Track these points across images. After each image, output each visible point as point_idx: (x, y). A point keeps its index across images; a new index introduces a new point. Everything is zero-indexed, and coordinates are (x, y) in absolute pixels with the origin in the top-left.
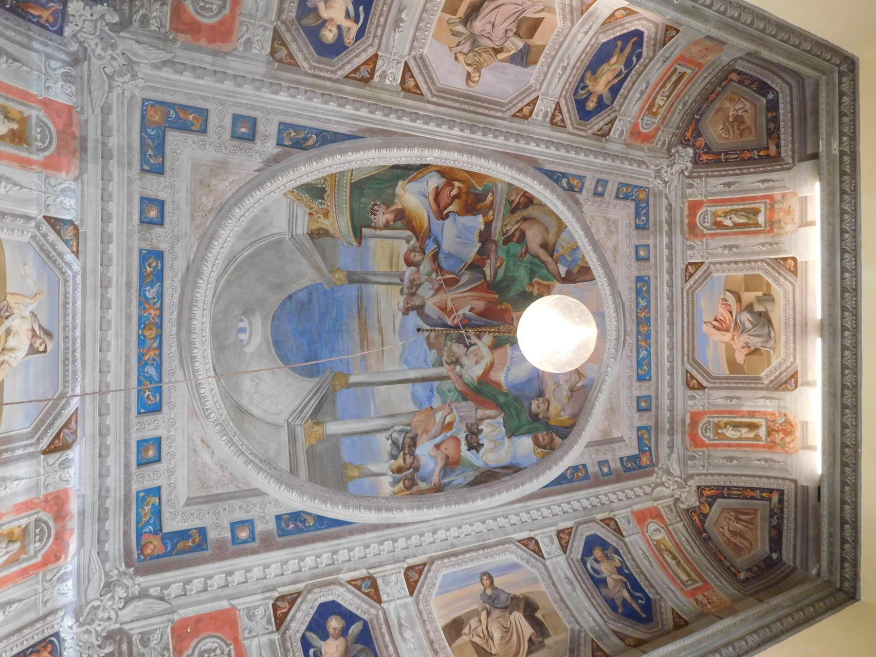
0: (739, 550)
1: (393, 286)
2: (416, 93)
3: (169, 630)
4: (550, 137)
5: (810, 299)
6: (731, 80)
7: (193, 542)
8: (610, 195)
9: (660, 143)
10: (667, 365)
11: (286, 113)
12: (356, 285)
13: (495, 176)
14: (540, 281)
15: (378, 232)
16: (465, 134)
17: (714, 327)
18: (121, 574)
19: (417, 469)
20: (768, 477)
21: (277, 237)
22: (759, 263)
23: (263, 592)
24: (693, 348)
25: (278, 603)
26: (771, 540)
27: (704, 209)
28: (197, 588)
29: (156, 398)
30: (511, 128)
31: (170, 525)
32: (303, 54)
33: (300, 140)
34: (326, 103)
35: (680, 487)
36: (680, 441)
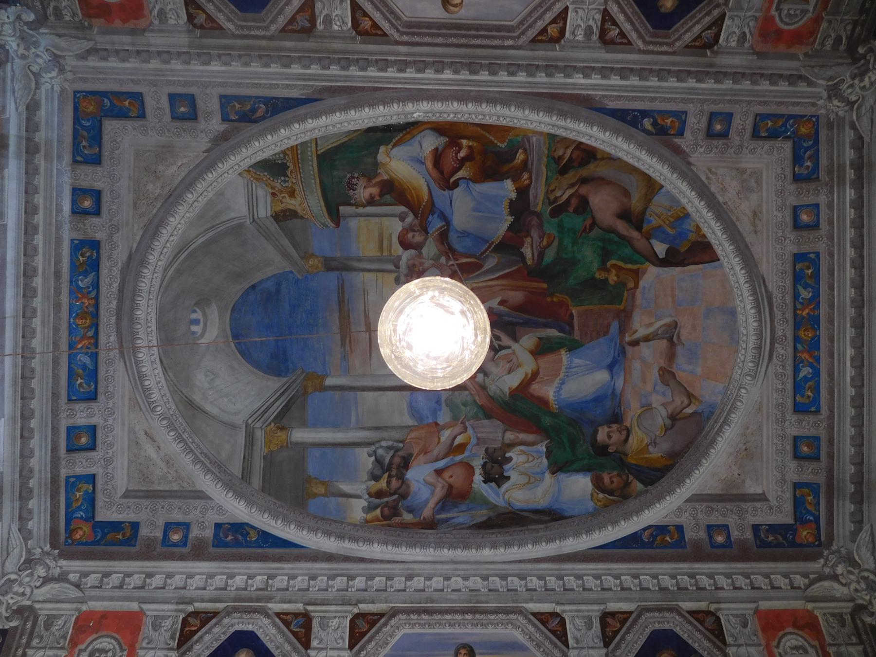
1: (385, 274)
2: (376, 35)
3: (73, 619)
4: (606, 61)
7: (123, 536)
9: (829, 43)
10: (851, 391)
12: (336, 273)
13: (525, 126)
14: (621, 264)
15: (361, 210)
19: (404, 496)
23: (177, 603)
25: (189, 619)
30: (534, 59)
31: (104, 514)
32: (225, 14)
33: (250, 113)
34: (267, 65)
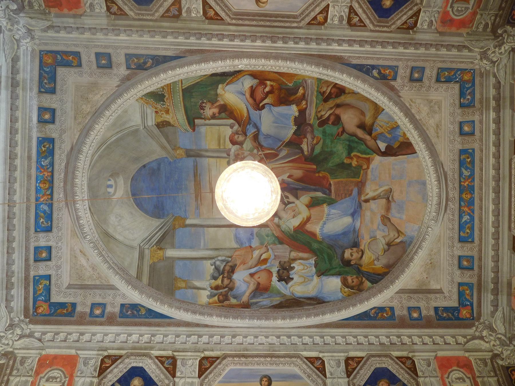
2: (217, 19)
3: (37, 359)
4: (351, 36)
7: (67, 310)
8: (430, 79)
9: (481, 27)
10: (492, 230)
11: (128, 48)
12: (193, 158)
13: (304, 74)
15: (207, 122)
16: (267, 45)
18: (20, 321)
19: (231, 289)
21: (134, 128)
28: (60, 338)
29: (48, 223)
31: (55, 298)
32: (128, 6)
33: (142, 64)
35: (503, 344)
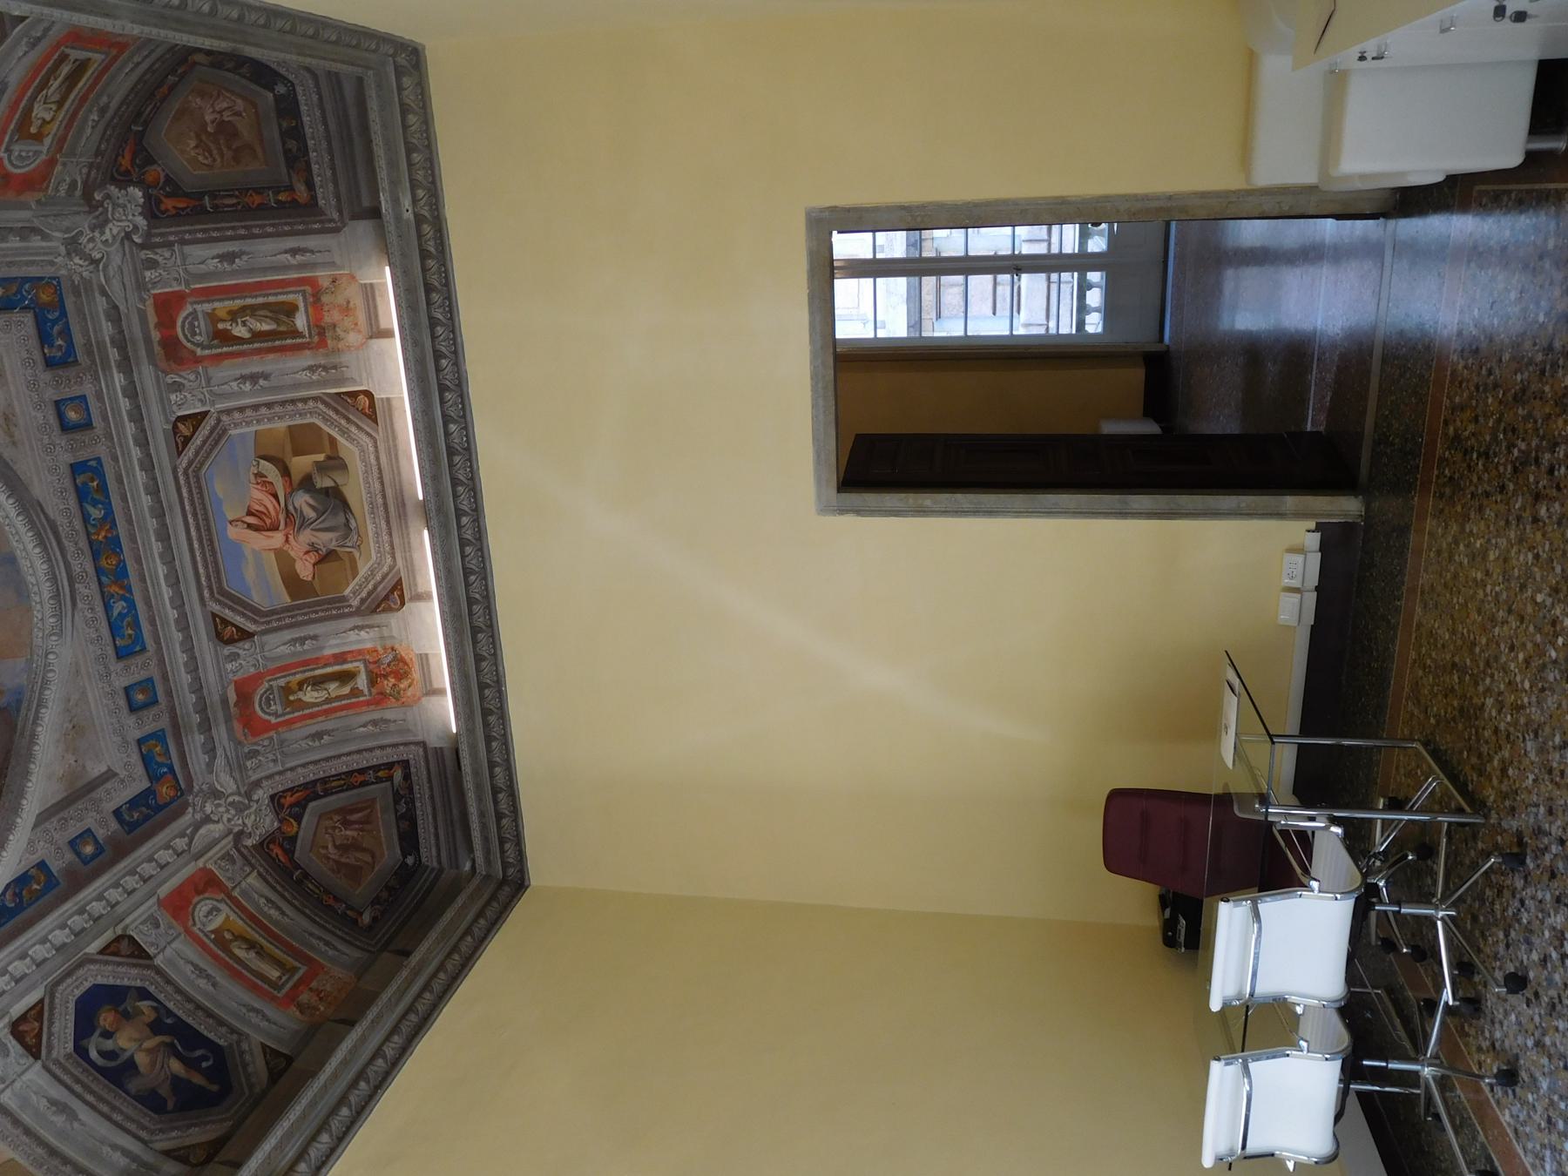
0: (354, 873)
5: (403, 462)
6: (195, 63)
9: (64, 188)
10: (173, 614)
17: (250, 526)
20: (382, 747)
22: (311, 403)
24: (218, 572)
26: (401, 838)
27: (189, 309)
35: (240, 809)
36: (224, 735)
